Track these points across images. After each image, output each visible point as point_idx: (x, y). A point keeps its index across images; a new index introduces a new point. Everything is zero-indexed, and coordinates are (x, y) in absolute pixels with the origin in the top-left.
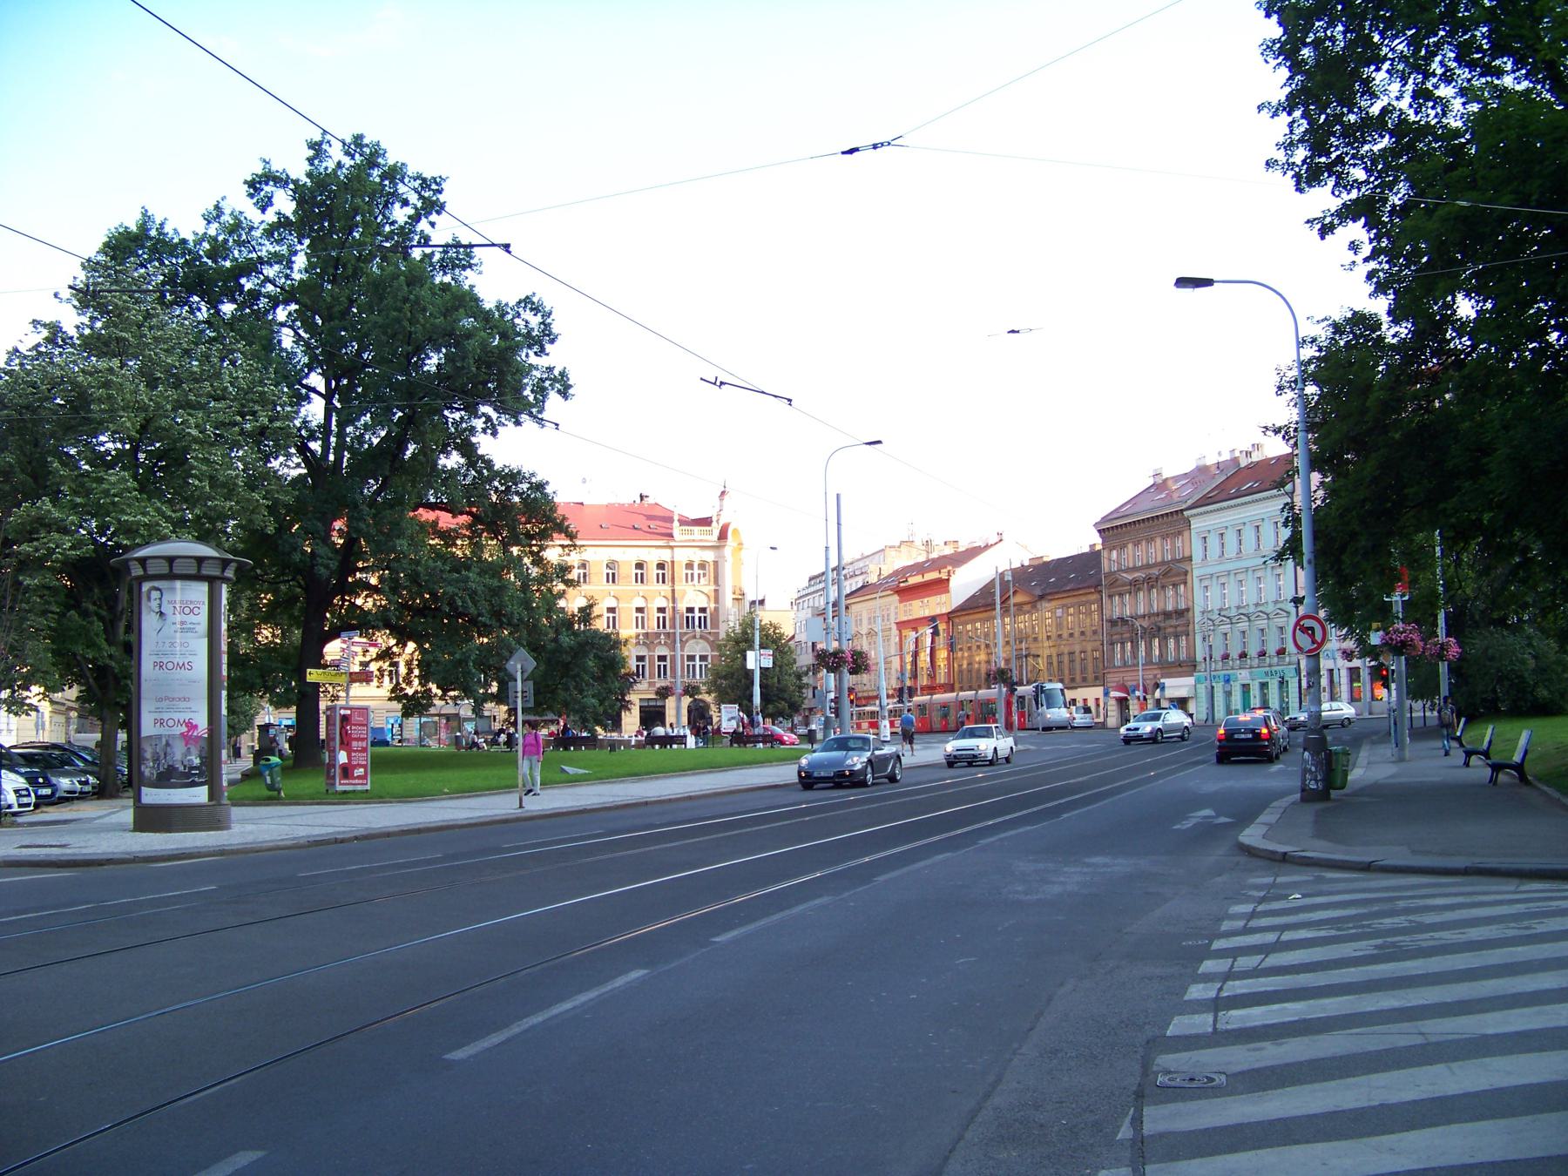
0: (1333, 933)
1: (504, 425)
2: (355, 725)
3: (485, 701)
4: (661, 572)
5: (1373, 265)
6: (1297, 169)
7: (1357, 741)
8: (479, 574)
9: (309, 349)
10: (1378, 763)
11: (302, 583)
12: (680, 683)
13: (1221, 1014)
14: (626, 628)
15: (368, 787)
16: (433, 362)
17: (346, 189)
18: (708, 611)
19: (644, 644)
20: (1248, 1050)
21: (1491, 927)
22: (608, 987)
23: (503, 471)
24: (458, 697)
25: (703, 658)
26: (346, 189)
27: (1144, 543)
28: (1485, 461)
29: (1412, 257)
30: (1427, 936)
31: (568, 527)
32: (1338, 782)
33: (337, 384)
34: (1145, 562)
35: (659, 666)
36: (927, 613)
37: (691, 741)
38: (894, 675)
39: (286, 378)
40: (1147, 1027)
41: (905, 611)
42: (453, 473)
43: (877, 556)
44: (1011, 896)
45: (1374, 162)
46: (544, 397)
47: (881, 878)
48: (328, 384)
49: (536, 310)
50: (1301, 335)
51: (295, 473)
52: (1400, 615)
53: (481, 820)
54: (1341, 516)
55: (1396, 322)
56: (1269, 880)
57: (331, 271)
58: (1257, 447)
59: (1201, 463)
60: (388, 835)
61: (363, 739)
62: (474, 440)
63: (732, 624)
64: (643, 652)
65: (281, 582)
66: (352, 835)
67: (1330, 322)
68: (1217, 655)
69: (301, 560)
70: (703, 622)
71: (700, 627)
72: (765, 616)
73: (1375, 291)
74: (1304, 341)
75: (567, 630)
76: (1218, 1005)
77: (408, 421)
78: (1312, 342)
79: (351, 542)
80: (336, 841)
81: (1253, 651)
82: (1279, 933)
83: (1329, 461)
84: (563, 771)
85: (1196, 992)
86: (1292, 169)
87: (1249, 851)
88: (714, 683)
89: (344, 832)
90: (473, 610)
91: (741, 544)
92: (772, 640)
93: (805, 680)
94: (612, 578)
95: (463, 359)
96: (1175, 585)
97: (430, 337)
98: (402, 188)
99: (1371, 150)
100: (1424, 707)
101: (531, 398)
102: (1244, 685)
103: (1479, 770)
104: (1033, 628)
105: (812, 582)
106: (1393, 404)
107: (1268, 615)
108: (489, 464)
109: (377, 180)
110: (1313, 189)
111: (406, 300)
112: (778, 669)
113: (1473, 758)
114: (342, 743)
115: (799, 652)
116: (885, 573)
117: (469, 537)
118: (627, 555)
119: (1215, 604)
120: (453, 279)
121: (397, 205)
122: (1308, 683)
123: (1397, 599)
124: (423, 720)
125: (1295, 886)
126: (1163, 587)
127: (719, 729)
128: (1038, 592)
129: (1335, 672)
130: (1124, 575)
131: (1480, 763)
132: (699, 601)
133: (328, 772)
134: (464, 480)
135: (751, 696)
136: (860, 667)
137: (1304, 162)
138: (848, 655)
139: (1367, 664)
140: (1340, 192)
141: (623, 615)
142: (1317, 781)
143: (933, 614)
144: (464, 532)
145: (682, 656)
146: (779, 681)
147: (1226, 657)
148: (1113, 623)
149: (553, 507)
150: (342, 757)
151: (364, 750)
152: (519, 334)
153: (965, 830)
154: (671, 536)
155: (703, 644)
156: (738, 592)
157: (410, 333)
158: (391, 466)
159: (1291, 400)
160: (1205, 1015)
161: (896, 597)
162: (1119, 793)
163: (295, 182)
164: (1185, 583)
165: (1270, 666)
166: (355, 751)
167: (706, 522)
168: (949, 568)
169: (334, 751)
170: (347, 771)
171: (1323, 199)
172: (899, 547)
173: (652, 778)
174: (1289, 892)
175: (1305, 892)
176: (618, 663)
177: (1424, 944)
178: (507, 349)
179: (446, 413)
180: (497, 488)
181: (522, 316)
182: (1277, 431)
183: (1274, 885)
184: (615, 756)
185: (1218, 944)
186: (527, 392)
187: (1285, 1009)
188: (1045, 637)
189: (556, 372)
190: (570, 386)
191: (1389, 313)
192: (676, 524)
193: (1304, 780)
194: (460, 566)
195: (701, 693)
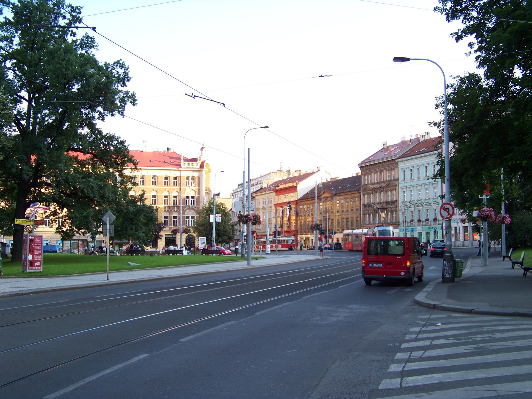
0: (455, 341)
1: (106, 115)
2: (36, 243)
3: (96, 234)
4: (175, 181)
5: (478, 53)
6: (447, 11)
7: (466, 257)
8: (95, 180)
9: (21, 80)
10: (475, 266)
11: (17, 182)
12: (181, 228)
13: (404, 379)
14: (160, 204)
15: (41, 270)
16: (76, 88)
17: (37, 9)
18: (195, 198)
19: (168, 211)
20: (416, 397)
21: (525, 340)
22: (130, 362)
23: (107, 135)
24: (84, 232)
25: (193, 218)
26: (37, 9)
27: (379, 173)
28: (524, 138)
29: (496, 51)
30: (497, 344)
31: (134, 160)
32: (458, 274)
33: (34, 96)
34: (379, 181)
35: (174, 221)
36: (287, 200)
37: (185, 252)
38: (273, 226)
39: (9, 92)
40: (370, 384)
41: (278, 200)
42: (85, 136)
43: (267, 176)
44: (314, 322)
45: (481, 9)
46: (125, 104)
47: (259, 313)
48: (29, 96)
49: (122, 66)
50: (446, 84)
51: (14, 134)
52: (486, 204)
53: (89, 285)
54: (462, 161)
55: (488, 78)
56: (428, 316)
57: (31, 45)
58: (427, 133)
59: (404, 140)
60: (47, 291)
61: (39, 250)
62: (94, 122)
63: (205, 203)
64: (167, 214)
65: (8, 181)
66: (30, 291)
67: (459, 78)
68: (408, 220)
69: (16, 172)
70: (193, 202)
71: (191, 204)
72: (219, 200)
73: (479, 66)
74: (448, 86)
75: (132, 204)
76: (403, 374)
77: (65, 112)
78: (451, 87)
79: (38, 164)
80: (22, 294)
81: (423, 219)
82: (431, 341)
83: (457, 137)
84: (129, 264)
85: (394, 368)
86: (445, 11)
87: (419, 304)
88: (197, 228)
89: (27, 290)
90: (92, 195)
91: (209, 170)
92: (221, 210)
93: (235, 227)
94: (155, 183)
95: (89, 86)
96: (391, 191)
97: (75, 76)
98: (62, 11)
99: (480, 3)
100: (495, 244)
101: (119, 104)
102: (419, 233)
103: (519, 271)
104: (332, 207)
105: (240, 187)
106: (485, 114)
107: (430, 204)
108: (100, 132)
109: (52, 6)
110: (454, 20)
111: (64, 60)
112: (224, 222)
113: (516, 265)
114: (30, 251)
115: (233, 216)
116: (270, 183)
117: (91, 164)
118: (161, 173)
119: (408, 199)
120: (86, 52)
121: (61, 18)
122: (446, 232)
123: (484, 197)
124: (72, 242)
125: (438, 319)
126: (386, 191)
127: (198, 248)
128: (334, 192)
129: (458, 228)
130: (370, 186)
131: (519, 267)
132: (191, 194)
133: (24, 264)
134: (90, 139)
135: (212, 234)
136: (257, 222)
137: (450, 8)
138: (252, 217)
139: (471, 225)
140: (466, 22)
141: (159, 199)
142: (449, 274)
143: (289, 201)
144: (89, 161)
145: (183, 217)
146: (224, 227)
147: (412, 221)
148: (365, 206)
149: (128, 152)
150: (30, 257)
151: (40, 254)
152: (114, 77)
153: (300, 291)
154: (180, 166)
155: (193, 211)
156: (208, 190)
157: (66, 74)
158: (57, 132)
159: (442, 111)
160: (396, 379)
161: (274, 194)
162: (354, 281)
163: (13, 4)
164: (396, 190)
165: (430, 225)
166: (36, 255)
167: (195, 160)
168: (297, 182)
169: (26, 255)
170: (32, 263)
171: (458, 25)
172: (276, 172)
173: (166, 268)
174: (436, 322)
175: (443, 322)
176: (154, 219)
177: (496, 348)
178: (108, 83)
179: (82, 110)
180: (103, 143)
181: (116, 69)
182: (435, 124)
183: (429, 319)
184: (152, 258)
185: (404, 346)
186: (117, 102)
187: (433, 377)
188: (336, 211)
189: (130, 94)
190: (136, 100)
191: (485, 74)
192: (182, 161)
193: (443, 273)
194: (87, 175)
195: (191, 232)
